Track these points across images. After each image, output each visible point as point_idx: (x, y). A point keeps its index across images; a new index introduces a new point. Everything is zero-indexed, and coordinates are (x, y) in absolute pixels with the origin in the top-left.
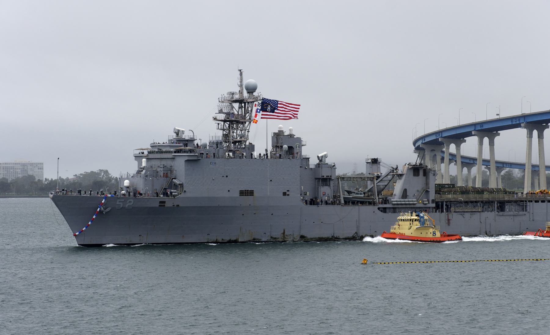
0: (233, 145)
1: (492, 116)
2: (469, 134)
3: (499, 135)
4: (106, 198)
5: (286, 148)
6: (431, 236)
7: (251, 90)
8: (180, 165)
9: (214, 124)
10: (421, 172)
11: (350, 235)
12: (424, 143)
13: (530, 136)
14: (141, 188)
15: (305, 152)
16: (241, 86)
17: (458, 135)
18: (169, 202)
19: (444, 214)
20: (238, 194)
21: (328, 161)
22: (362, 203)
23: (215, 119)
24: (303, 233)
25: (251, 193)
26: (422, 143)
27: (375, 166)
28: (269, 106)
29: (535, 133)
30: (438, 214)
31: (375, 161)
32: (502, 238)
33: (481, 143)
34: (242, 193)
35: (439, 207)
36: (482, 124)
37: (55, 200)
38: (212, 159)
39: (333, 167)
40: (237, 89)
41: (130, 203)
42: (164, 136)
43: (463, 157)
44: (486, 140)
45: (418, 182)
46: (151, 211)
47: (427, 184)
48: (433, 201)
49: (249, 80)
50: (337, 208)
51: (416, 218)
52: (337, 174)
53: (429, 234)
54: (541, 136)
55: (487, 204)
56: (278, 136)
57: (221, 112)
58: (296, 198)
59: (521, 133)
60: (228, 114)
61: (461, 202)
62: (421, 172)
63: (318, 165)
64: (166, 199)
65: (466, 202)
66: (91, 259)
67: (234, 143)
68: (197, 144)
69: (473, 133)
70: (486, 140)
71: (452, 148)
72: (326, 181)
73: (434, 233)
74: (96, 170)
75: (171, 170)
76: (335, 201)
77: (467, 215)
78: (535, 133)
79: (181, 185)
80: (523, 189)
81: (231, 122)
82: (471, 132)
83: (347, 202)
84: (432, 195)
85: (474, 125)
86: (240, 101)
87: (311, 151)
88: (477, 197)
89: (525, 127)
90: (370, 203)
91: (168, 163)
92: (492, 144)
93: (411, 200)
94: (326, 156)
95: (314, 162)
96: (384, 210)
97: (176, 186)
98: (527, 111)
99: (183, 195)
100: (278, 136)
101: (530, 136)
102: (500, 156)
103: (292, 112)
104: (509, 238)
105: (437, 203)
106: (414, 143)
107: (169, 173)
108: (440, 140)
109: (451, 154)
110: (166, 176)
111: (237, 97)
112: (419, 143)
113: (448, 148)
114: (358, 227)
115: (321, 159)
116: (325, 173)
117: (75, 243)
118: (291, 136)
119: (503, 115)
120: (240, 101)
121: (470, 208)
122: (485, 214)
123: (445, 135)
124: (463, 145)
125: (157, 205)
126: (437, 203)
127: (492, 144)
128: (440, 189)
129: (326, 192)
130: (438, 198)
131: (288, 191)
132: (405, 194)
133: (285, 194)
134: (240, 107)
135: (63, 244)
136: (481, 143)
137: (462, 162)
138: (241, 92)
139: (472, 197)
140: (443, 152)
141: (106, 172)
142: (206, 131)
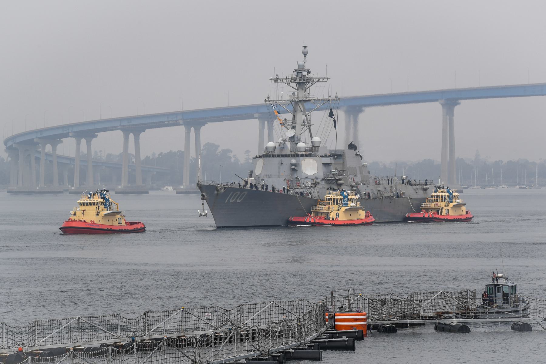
2: (66, 135)
3: (62, 142)
12: (40, 138)
17: (55, 136)
26: (37, 137)
32: (448, 127)
33: (78, 144)
43: (59, 157)
51: (102, 200)
59: (181, 130)
66: (64, 237)
69: (70, 134)
71: (48, 148)
78: (131, 136)
82: (68, 133)
89: (73, 136)
98: (73, 121)
106: (6, 142)
108: (35, 140)
109: (47, 155)
112: (10, 144)
113: (44, 148)
123: (18, 140)
124: (94, 141)
131: (317, 178)
136: (78, 144)
137: (58, 163)
140: (39, 152)
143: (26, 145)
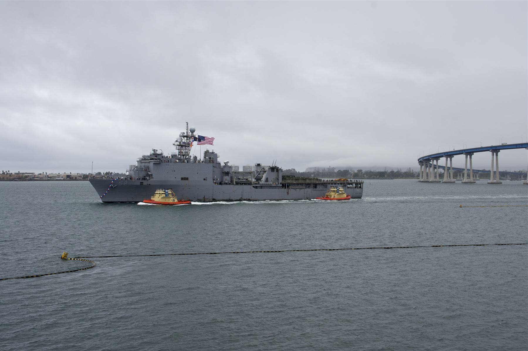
0: (183, 158)
1: (452, 150)
2: (442, 156)
4: (114, 180)
5: (211, 157)
6: (172, 201)
7: (193, 131)
8: (151, 165)
9: (174, 147)
10: (275, 170)
11: (238, 199)
13: (467, 157)
14: (133, 176)
15: (219, 160)
16: (187, 129)
17: (437, 157)
18: (145, 183)
19: (286, 190)
20: (180, 179)
21: (229, 164)
22: (245, 184)
23: (174, 145)
24: (214, 198)
25: (187, 179)
27: (259, 167)
28: (200, 139)
29: (469, 156)
30: (283, 189)
31: (259, 165)
33: (447, 160)
34: (182, 179)
35: (284, 186)
36: (447, 153)
37: (91, 181)
38: (166, 163)
39: (231, 167)
40: (185, 131)
41: (126, 183)
42: (148, 153)
44: (449, 159)
45: (274, 175)
46: (136, 187)
47: (278, 175)
48: (281, 183)
49: (191, 127)
50: (232, 186)
52: (233, 171)
53: (171, 200)
54: (471, 158)
55: (308, 185)
56: (207, 153)
57: (177, 141)
58: (210, 181)
59: (463, 156)
60: (180, 142)
61: (294, 184)
62: (275, 170)
63: (224, 166)
64: (143, 181)
65: (298, 184)
67: (184, 155)
68: (195, 158)
70: (449, 159)
72: (227, 174)
73: (174, 200)
74: (290, 169)
75: (148, 167)
76: (231, 183)
77: (298, 190)
78: (469, 156)
79: (152, 175)
80: (367, 179)
81: (182, 146)
83: (237, 183)
84: (280, 181)
85: (444, 153)
86: (187, 137)
87: (221, 160)
88: (303, 182)
90: (249, 184)
91: (146, 164)
92: (451, 160)
93: (270, 183)
94: (228, 162)
95: (222, 164)
96: (256, 187)
97: (149, 175)
98: (465, 148)
99: (152, 179)
100: (207, 153)
101: (467, 157)
102: (439, 164)
103: (211, 141)
104: (144, 204)
105: (283, 184)
106: (418, 160)
107: (147, 169)
110: (146, 170)
111: (185, 134)
114: (242, 195)
115: (226, 163)
116: (226, 170)
117: (101, 201)
118: (213, 153)
119: (455, 150)
120: (187, 137)
121: (300, 186)
122: (307, 189)
124: (439, 161)
125: (139, 184)
126: (283, 184)
127: (451, 160)
128: (284, 178)
129: (227, 179)
130: (284, 182)
132: (267, 180)
133: (204, 179)
134: (187, 139)
135: (95, 201)
136: (447, 160)
138: (187, 133)
139: (300, 182)
141: (294, 169)
142: (169, 150)
143: (425, 161)
